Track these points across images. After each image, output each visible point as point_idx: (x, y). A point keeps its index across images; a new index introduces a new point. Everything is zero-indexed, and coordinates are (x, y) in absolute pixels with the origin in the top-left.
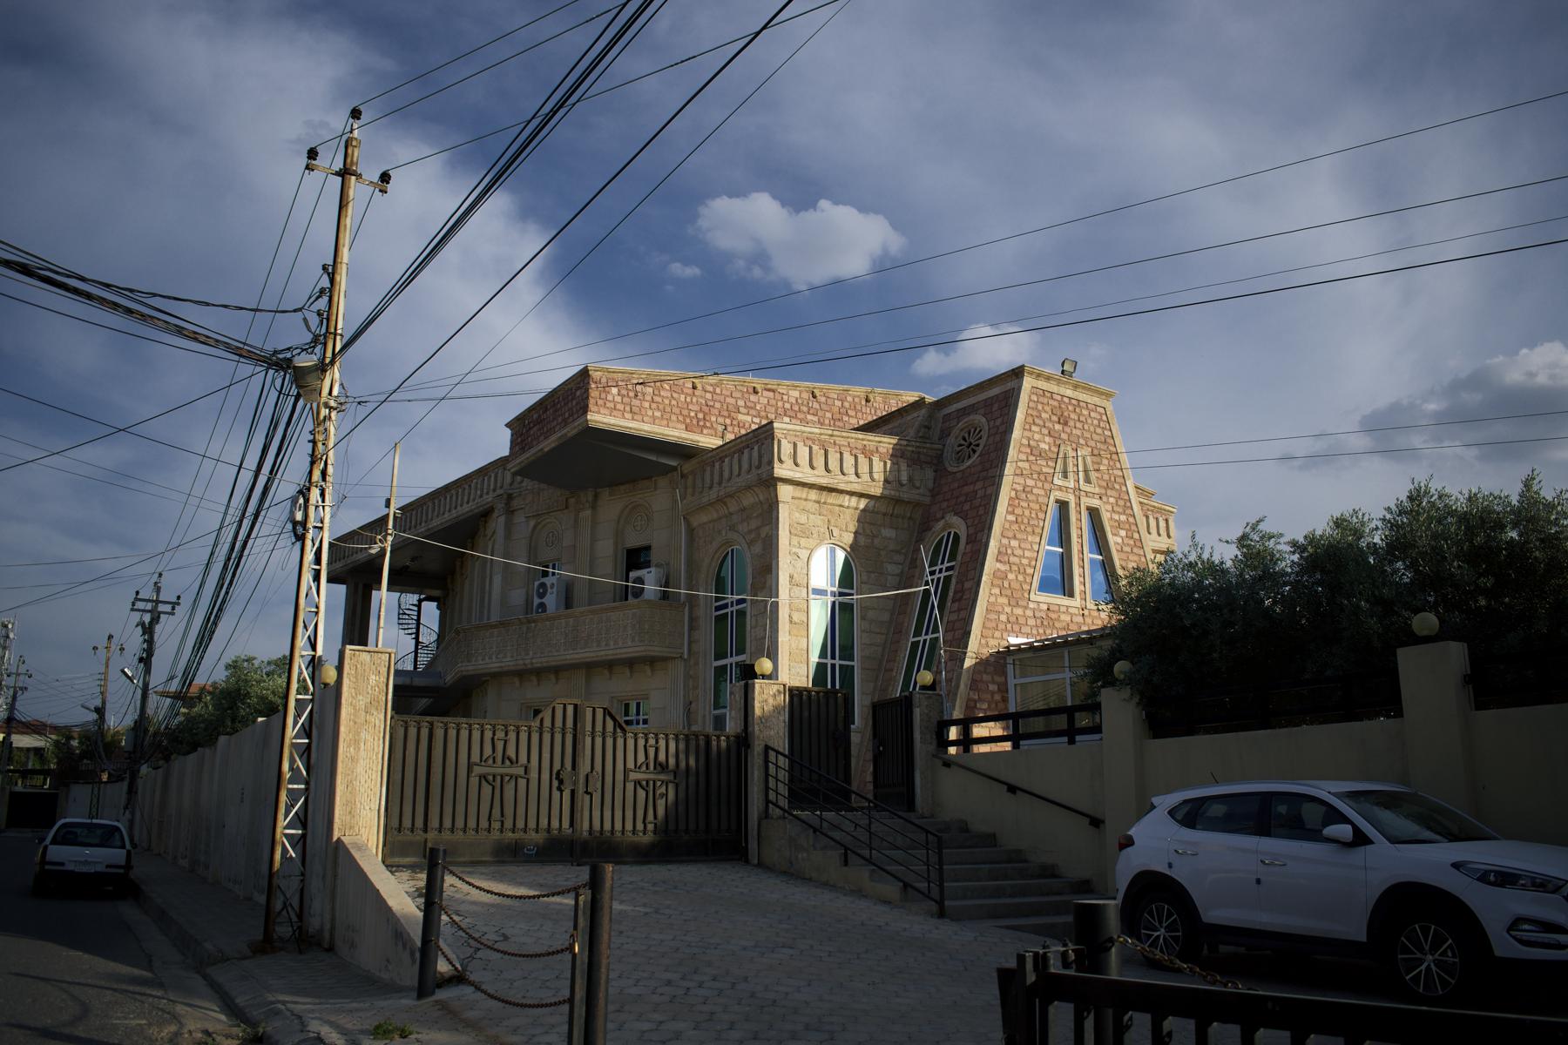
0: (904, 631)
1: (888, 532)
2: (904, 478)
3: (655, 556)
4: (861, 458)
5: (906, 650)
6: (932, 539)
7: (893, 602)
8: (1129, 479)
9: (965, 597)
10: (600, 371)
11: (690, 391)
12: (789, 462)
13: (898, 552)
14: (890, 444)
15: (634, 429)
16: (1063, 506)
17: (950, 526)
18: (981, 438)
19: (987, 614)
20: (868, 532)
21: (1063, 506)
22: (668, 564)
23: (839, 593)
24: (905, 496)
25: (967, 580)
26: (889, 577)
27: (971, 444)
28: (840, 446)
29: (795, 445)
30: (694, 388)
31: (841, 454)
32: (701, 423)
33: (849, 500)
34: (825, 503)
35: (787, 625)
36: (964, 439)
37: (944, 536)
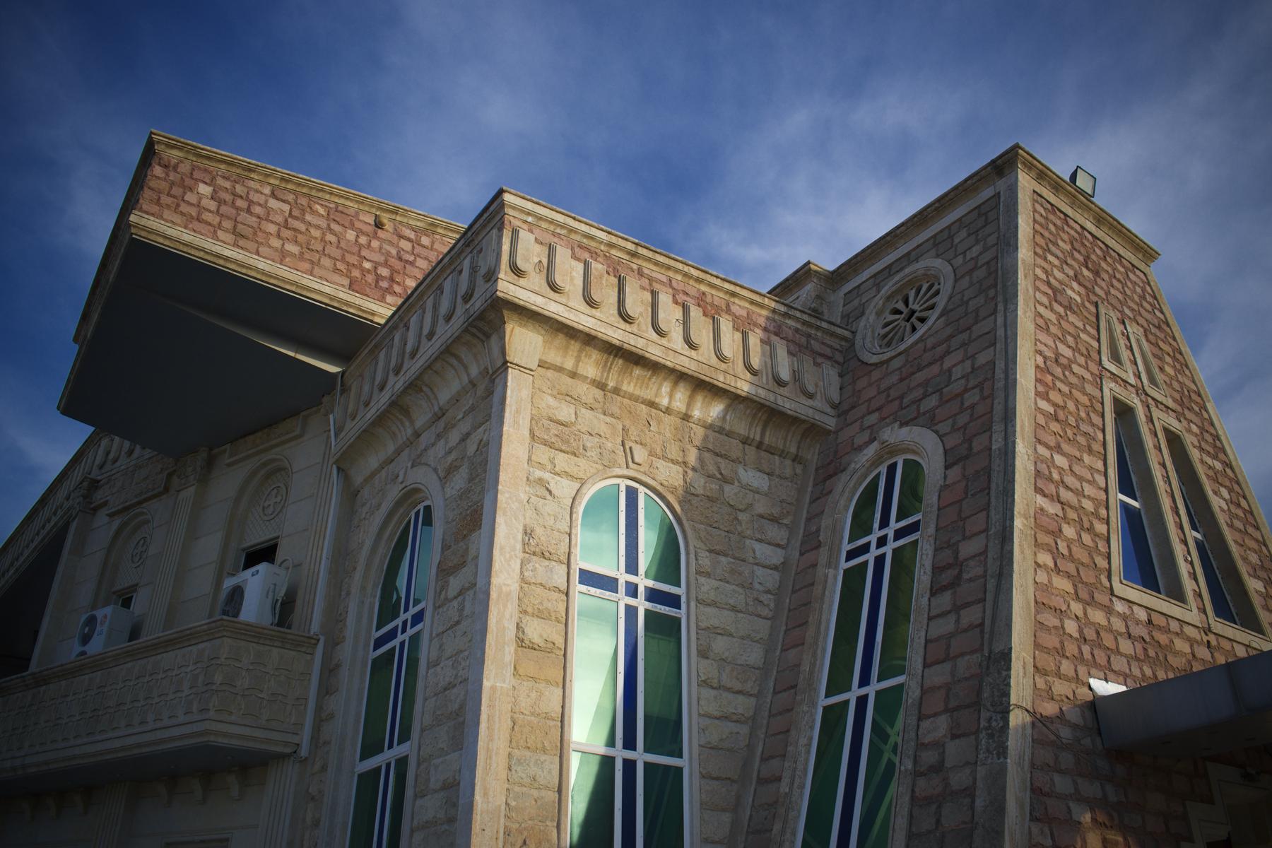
1: (750, 477)
2: (785, 374)
3: (280, 555)
4: (695, 313)
5: (812, 728)
8: (1209, 401)
9: (965, 576)
10: (180, 149)
11: (370, 229)
12: (536, 280)
13: (774, 520)
15: (235, 261)
16: (1123, 412)
18: (932, 307)
19: (1037, 612)
20: (712, 469)
21: (1123, 412)
22: (298, 566)
24: (788, 406)
25: (964, 538)
26: (760, 572)
27: (913, 312)
28: (651, 279)
29: (551, 251)
30: (379, 225)
31: (654, 294)
32: (384, 284)
33: (671, 396)
34: (616, 391)
35: (510, 649)
36: (906, 303)
37: (878, 475)
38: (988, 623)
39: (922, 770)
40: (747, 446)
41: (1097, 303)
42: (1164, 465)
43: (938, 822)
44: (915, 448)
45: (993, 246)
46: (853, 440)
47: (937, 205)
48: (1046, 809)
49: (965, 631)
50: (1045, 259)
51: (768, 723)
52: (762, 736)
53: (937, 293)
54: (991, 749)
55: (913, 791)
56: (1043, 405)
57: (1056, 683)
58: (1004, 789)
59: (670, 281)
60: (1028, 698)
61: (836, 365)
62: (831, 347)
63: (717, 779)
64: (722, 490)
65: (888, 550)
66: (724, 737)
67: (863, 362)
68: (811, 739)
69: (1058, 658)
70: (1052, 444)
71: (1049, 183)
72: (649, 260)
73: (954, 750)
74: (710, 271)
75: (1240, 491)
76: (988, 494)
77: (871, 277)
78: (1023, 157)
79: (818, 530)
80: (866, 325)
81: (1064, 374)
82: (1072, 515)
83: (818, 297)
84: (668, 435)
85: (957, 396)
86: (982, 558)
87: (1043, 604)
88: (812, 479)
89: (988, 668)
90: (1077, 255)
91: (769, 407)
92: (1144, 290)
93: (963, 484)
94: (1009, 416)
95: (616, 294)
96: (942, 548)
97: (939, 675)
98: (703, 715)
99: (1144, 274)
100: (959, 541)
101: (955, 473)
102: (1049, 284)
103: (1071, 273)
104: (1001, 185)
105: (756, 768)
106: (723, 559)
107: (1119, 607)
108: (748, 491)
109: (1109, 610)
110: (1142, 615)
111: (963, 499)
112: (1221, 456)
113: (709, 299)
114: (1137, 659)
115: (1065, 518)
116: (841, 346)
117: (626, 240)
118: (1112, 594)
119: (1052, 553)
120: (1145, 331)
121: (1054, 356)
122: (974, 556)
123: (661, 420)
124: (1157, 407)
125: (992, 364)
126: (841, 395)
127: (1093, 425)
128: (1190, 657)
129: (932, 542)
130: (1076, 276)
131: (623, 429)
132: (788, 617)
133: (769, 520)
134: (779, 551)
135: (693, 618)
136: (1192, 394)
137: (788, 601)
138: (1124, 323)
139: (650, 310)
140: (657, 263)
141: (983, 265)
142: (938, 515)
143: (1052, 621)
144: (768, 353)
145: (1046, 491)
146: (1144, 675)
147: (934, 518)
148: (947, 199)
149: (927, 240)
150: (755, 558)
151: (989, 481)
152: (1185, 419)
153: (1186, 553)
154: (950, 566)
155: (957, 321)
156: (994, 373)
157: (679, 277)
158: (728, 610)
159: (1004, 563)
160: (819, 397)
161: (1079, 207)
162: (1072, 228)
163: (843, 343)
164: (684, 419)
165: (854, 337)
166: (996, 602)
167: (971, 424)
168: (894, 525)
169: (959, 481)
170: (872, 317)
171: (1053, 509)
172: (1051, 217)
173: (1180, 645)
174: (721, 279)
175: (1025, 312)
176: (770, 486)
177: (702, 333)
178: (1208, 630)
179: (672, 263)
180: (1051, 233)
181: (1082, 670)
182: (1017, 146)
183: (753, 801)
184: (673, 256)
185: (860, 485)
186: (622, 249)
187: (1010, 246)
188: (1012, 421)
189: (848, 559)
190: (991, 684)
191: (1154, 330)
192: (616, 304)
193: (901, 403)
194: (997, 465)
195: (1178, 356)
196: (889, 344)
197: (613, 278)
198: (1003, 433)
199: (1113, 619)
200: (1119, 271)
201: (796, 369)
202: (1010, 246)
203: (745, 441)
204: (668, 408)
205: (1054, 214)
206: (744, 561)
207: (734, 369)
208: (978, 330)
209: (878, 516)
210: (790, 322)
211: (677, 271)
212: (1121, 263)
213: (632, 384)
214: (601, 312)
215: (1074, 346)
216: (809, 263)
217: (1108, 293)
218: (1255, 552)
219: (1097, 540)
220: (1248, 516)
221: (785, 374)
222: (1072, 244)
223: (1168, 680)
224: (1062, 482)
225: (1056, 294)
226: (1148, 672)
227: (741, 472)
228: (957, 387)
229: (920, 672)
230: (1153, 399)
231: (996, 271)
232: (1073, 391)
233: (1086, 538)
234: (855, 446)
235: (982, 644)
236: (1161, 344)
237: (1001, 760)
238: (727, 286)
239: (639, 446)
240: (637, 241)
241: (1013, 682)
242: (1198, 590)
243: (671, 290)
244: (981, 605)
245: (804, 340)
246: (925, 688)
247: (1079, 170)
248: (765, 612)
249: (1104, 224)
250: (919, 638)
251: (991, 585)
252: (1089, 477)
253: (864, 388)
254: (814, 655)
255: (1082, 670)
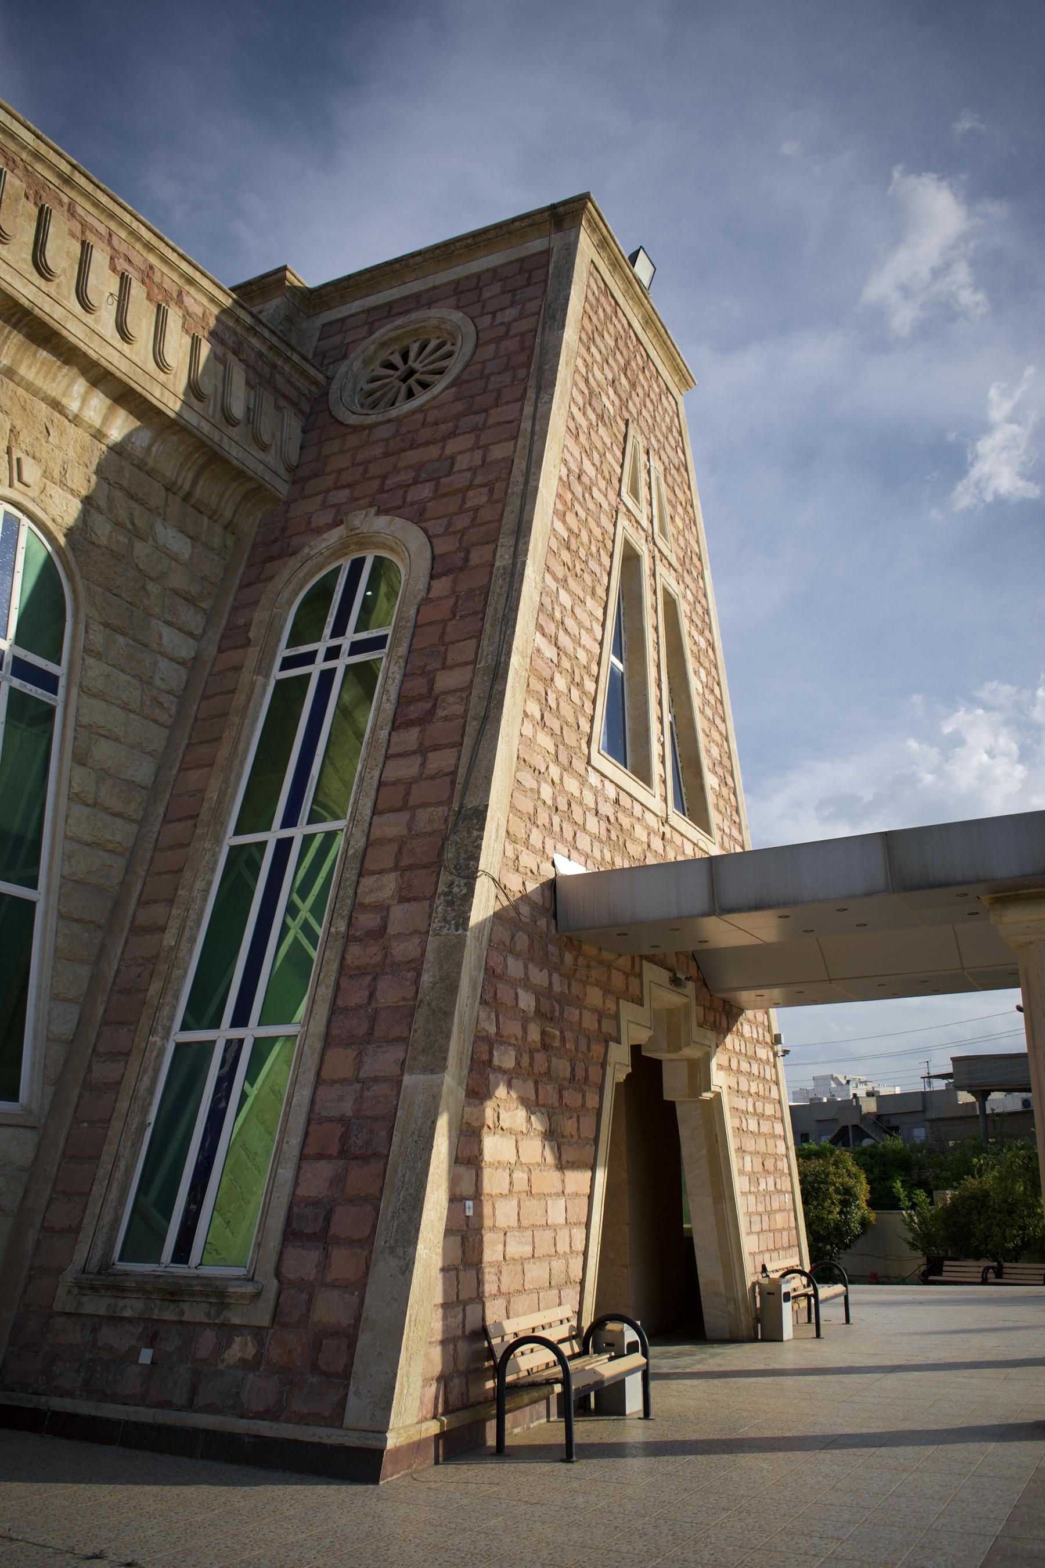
0: (205, 815)
2: (238, 410)
5: (213, 870)
6: (301, 574)
7: (167, 732)
9: (440, 713)
13: (191, 601)
14: (213, 300)
16: (631, 558)
17: (363, 541)
18: (441, 372)
19: (518, 770)
20: (122, 515)
21: (631, 558)
23: (16, 660)
24: (234, 453)
25: (444, 667)
26: (163, 663)
27: (412, 372)
28: (84, 225)
31: (86, 248)
33: (84, 400)
36: (405, 357)
37: (338, 570)
38: (462, 772)
39: (358, 934)
40: (171, 495)
41: (627, 421)
42: (656, 629)
43: (371, 996)
44: (394, 544)
45: (534, 314)
46: (311, 517)
47: (469, 241)
48: (495, 992)
49: (432, 778)
50: (588, 349)
51: (152, 857)
52: (143, 873)
53: (450, 355)
54: (449, 919)
55: (343, 958)
56: (559, 526)
57: (523, 853)
58: (459, 965)
59: (110, 235)
60: (496, 866)
61: (300, 416)
62: (298, 389)
63: (78, 921)
64: (131, 546)
65: (340, 664)
66: (94, 868)
67: (337, 420)
68: (210, 883)
69: (529, 825)
70: (560, 576)
71: (609, 256)
72: (87, 195)
73: (400, 916)
74: (166, 239)
75: (716, 677)
76: (483, 619)
77: (363, 312)
78: (590, 213)
79: (248, 625)
80: (347, 373)
81: (583, 496)
82: (566, 664)
83: (288, 318)
84: (71, 453)
85: (458, 490)
86: (464, 695)
87: (524, 760)
88: (246, 557)
89: (456, 825)
90: (618, 355)
91: (211, 448)
92: (672, 421)
93: (453, 600)
94: (522, 530)
95: (34, 231)
96: (412, 674)
97: (392, 826)
98: (71, 839)
99: (676, 402)
100: (438, 670)
101: (442, 586)
102: (587, 381)
103: (610, 377)
104: (557, 240)
105: (131, 912)
106: (121, 640)
107: (594, 779)
108: (163, 555)
109: (583, 781)
110: (611, 792)
111: (450, 619)
112: (707, 632)
113: (157, 278)
114: (598, 839)
115: (558, 666)
116: (310, 391)
117: (60, 155)
118: (589, 763)
119: (540, 703)
120: (665, 469)
121: (577, 471)
122: (455, 691)
123: (65, 431)
124: (661, 560)
125: (509, 463)
126: (300, 456)
127: (601, 565)
128: (646, 847)
129: (403, 664)
130: (613, 382)
131: (11, 431)
132: (192, 730)
133: (184, 598)
134: (190, 641)
135: (72, 709)
136: (694, 556)
137: (195, 707)
138: (648, 453)
139: (77, 267)
140: (97, 204)
141: (516, 336)
142: (414, 633)
143: (529, 781)
144: (221, 376)
145: (546, 630)
146: (603, 859)
147: (409, 635)
148: (484, 237)
149: (447, 284)
150: (160, 644)
151: (486, 604)
152: (683, 582)
153: (660, 732)
154: (420, 698)
155: (471, 397)
156: (511, 472)
157: (123, 234)
158: (118, 706)
159: (492, 705)
160: (273, 452)
161: (632, 299)
162: (620, 321)
163: (313, 388)
164: (95, 437)
165: (329, 384)
166: (475, 750)
167: (471, 530)
168: (351, 636)
169: (447, 597)
170: (357, 365)
171: (550, 652)
172: (603, 300)
173: (640, 833)
174: (179, 254)
175: (559, 408)
176: (192, 554)
177: (141, 323)
178: (666, 821)
179: (118, 210)
180: (599, 319)
181: (549, 843)
182: (585, 198)
183: (123, 953)
184: (121, 200)
185: (313, 576)
186: (52, 167)
187: (556, 320)
188: (525, 536)
189: (283, 668)
190: (457, 843)
191: (673, 471)
192: (32, 246)
193: (382, 484)
194: (498, 585)
195: (689, 508)
196: (374, 406)
197: (32, 206)
198: (512, 549)
199: (586, 792)
200: (653, 390)
201: (252, 406)
202: (556, 320)
203: (170, 488)
204: (76, 416)
205: (606, 297)
206: (145, 645)
207: (174, 385)
208: (496, 415)
209: (331, 620)
210: (254, 341)
211: (122, 224)
212: (657, 381)
213: (34, 370)
214: (9, 251)
215: (598, 465)
216: (285, 268)
217: (640, 413)
218: (718, 745)
219: (584, 699)
220: (719, 705)
221: (238, 410)
222: (616, 341)
223: (623, 870)
224: (562, 623)
225: (592, 396)
226: (608, 857)
227: (159, 527)
228: (459, 480)
229: (368, 819)
230: (660, 551)
231: (533, 348)
232: (590, 519)
233: (575, 694)
234: (313, 526)
235: (451, 796)
236: (677, 489)
237: (459, 932)
238: (184, 266)
239: (30, 460)
240: (75, 162)
241: (485, 844)
242: (663, 776)
243: (109, 248)
244: (455, 749)
245: (267, 371)
246: (372, 838)
247: (641, 251)
248: (164, 718)
249: (651, 328)
250: (371, 778)
251: (472, 727)
252: (588, 624)
253: (334, 454)
254: (226, 781)
255: (549, 843)
